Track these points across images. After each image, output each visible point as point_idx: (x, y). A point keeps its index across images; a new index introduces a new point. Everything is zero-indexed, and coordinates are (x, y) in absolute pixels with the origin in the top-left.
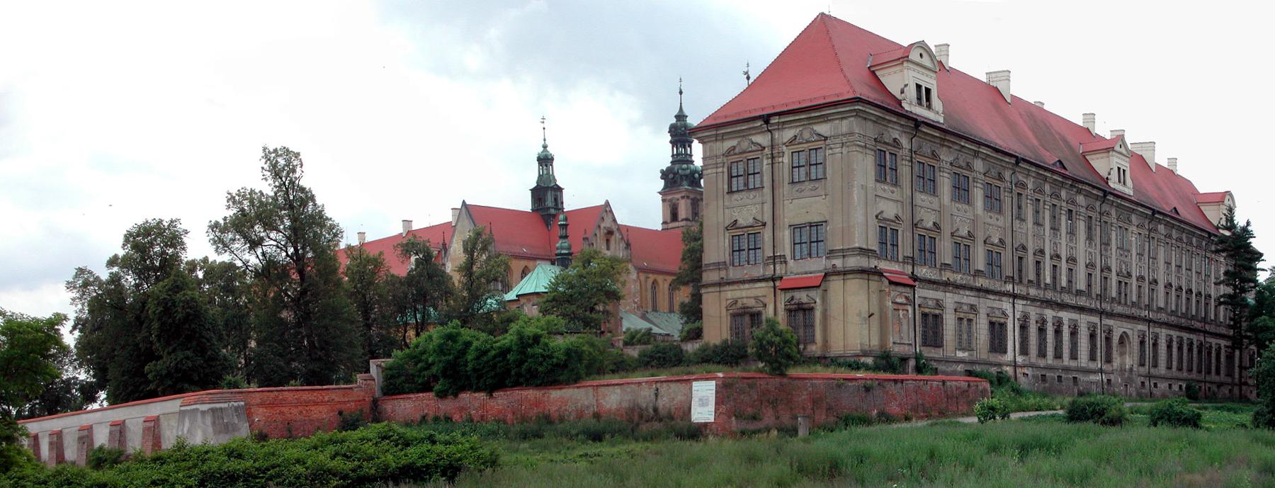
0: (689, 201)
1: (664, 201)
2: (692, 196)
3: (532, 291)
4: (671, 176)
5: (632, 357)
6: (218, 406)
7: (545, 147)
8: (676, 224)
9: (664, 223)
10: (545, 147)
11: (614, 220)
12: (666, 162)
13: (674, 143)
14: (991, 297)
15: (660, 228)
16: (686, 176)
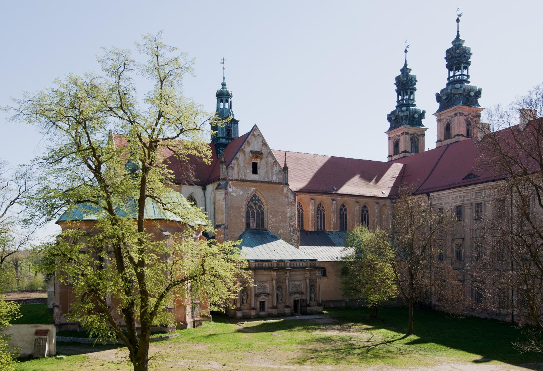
0: (408, 137)
1: (438, 121)
7: (224, 85)
9: (390, 156)
10: (224, 85)
11: (265, 144)
12: (392, 106)
13: (399, 92)
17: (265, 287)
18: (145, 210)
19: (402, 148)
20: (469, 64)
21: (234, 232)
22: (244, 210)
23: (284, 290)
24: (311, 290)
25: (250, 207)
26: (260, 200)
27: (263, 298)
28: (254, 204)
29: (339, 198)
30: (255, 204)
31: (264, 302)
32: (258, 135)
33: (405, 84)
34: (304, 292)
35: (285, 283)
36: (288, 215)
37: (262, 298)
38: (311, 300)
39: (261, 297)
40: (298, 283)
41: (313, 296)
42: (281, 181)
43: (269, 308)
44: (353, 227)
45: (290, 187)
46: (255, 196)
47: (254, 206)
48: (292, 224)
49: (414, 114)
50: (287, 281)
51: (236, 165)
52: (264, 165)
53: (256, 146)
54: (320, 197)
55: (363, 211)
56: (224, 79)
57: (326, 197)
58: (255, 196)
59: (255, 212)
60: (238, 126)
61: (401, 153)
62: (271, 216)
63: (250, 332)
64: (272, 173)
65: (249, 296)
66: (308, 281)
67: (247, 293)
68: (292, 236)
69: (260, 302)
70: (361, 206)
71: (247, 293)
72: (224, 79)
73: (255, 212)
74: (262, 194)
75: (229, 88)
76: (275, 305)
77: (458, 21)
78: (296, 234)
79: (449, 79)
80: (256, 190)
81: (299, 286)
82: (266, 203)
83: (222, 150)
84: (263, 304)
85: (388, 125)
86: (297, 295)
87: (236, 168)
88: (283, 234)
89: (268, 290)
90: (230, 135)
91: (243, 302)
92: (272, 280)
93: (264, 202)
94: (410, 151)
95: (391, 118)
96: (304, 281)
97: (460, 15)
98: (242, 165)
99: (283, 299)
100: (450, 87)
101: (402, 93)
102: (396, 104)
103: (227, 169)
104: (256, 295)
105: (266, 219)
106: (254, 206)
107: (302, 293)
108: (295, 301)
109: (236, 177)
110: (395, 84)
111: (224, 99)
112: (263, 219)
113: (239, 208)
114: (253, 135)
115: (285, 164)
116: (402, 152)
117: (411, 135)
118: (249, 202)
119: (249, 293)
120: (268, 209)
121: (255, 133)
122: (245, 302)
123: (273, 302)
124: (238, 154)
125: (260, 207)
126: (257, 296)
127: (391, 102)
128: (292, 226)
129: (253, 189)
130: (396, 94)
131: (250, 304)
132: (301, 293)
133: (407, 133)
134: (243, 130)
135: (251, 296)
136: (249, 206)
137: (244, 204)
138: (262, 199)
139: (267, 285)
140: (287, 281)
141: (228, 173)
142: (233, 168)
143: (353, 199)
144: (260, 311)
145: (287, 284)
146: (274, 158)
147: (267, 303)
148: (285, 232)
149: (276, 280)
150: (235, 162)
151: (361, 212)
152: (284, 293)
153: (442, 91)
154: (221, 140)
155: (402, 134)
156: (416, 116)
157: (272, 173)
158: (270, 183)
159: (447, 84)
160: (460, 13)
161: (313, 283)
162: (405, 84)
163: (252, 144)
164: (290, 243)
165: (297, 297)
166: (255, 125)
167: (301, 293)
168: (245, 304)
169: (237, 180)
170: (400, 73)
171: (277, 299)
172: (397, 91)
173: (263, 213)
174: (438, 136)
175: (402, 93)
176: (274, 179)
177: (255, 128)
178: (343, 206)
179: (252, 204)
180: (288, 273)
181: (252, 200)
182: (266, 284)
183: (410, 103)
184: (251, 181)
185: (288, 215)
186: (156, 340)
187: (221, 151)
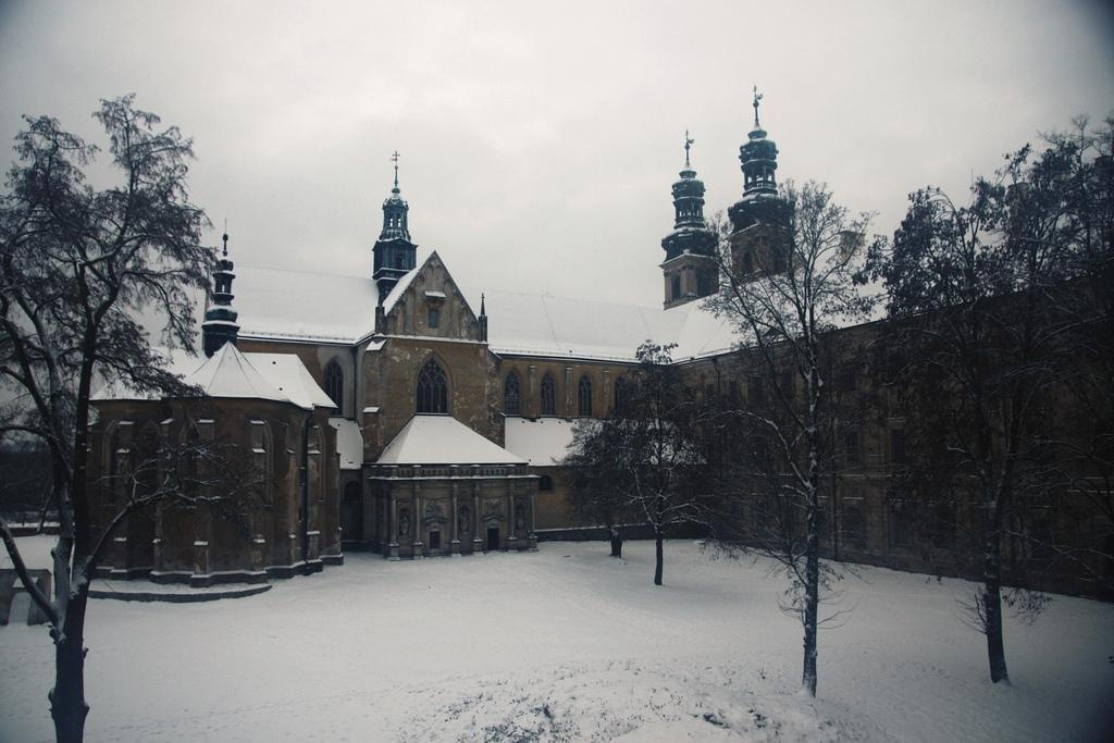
0: (692, 272)
1: (666, 275)
7: (396, 191)
10: (396, 191)
12: (668, 226)
17: (438, 509)
20: (775, 166)
22: (412, 384)
27: (435, 527)
30: (432, 374)
31: (497, 530)
33: (688, 195)
35: (473, 501)
36: (487, 391)
39: (433, 525)
40: (495, 501)
41: (521, 522)
44: (59, 555)
46: (432, 361)
48: (493, 406)
50: (477, 499)
51: (401, 314)
55: (617, 385)
56: (396, 182)
63: (917, 572)
64: (460, 325)
66: (512, 498)
69: (431, 533)
72: (396, 182)
73: (432, 386)
74: (442, 359)
75: (403, 196)
77: (756, 105)
80: (434, 353)
81: (497, 505)
88: (477, 423)
89: (445, 513)
91: (401, 533)
92: (451, 496)
93: (447, 372)
97: (691, 142)
98: (410, 313)
104: (422, 521)
105: (449, 398)
108: (490, 530)
115: (483, 312)
119: (412, 517)
120: (452, 382)
121: (433, 263)
122: (405, 532)
125: (440, 379)
127: (666, 221)
128: (493, 410)
129: (428, 351)
130: (674, 208)
133: (691, 267)
135: (416, 522)
136: (422, 379)
137: (413, 374)
138: (444, 367)
139: (443, 505)
140: (477, 499)
141: (386, 326)
144: (431, 547)
145: (477, 504)
146: (463, 301)
149: (458, 496)
151: (613, 385)
152: (471, 519)
155: (684, 268)
157: (460, 325)
160: (758, 93)
162: (688, 195)
164: (489, 439)
166: (435, 253)
168: (465, 533)
173: (444, 386)
178: (585, 377)
181: (426, 367)
182: (440, 504)
183: (698, 220)
185: (487, 391)
186: (102, 596)
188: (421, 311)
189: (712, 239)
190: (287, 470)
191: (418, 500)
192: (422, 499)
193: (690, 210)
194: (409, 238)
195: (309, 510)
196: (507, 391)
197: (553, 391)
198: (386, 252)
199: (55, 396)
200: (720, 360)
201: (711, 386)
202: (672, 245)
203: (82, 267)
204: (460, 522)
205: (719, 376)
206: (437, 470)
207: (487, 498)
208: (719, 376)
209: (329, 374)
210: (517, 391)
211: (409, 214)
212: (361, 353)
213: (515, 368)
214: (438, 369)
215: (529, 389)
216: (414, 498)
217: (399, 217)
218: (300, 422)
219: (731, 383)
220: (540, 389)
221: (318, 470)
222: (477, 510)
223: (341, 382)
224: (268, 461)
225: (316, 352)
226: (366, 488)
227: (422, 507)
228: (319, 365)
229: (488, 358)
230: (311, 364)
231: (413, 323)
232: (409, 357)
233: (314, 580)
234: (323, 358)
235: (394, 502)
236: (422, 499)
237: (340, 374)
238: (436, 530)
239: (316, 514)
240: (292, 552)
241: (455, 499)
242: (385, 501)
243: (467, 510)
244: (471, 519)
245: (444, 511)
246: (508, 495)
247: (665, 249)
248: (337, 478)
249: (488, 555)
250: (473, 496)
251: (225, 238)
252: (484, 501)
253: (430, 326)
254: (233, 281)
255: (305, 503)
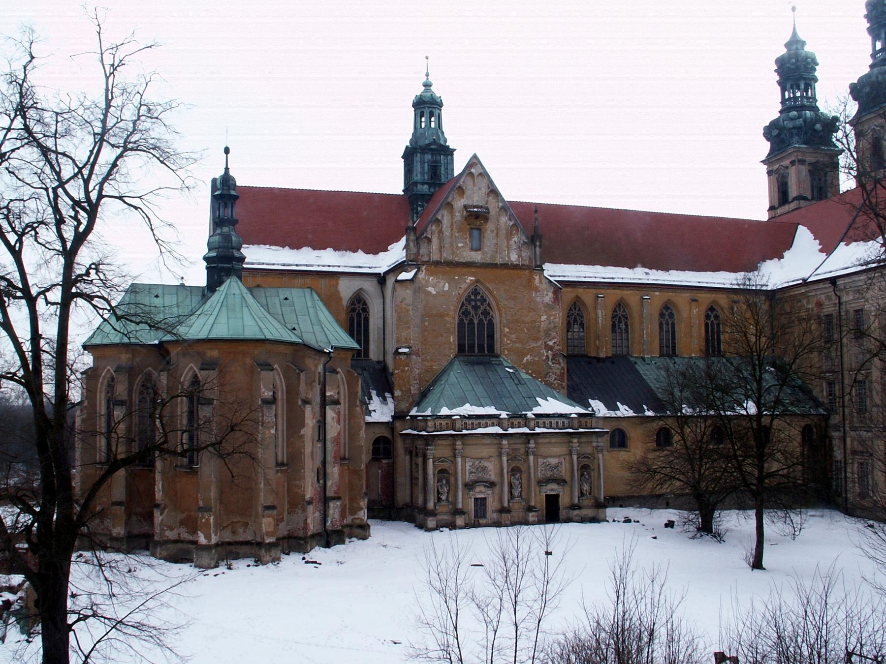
0: (804, 169)
1: (769, 173)
2: (810, 159)
3: (203, 335)
4: (775, 132)
5: (341, 474)
6: (469, 432)
7: (427, 85)
8: (786, 208)
9: (772, 208)
10: (427, 85)
11: (494, 192)
12: (772, 110)
13: (783, 85)
14: (319, 445)
15: (764, 216)
16: (799, 128)
17: (484, 469)
18: (754, 551)
19: (793, 192)
21: (432, 361)
22: (452, 320)
23: (524, 476)
24: (582, 475)
25: (466, 313)
26: (485, 300)
27: (480, 492)
28: (473, 307)
29: (657, 293)
30: (476, 308)
32: (481, 174)
33: (796, 72)
34: (568, 479)
35: (527, 461)
37: (480, 492)
38: (582, 494)
39: (478, 489)
40: (554, 461)
41: (586, 487)
42: (527, 263)
43: (493, 512)
45: (546, 274)
46: (476, 292)
47: (472, 312)
48: (551, 343)
49: (814, 125)
50: (531, 458)
52: (492, 231)
53: (475, 197)
54: (619, 292)
55: (707, 317)
56: (427, 75)
57: (628, 292)
58: (476, 292)
59: (476, 322)
60: (452, 160)
61: (792, 201)
62: (507, 330)
65: (453, 488)
66: (575, 457)
67: (448, 482)
68: (550, 368)
69: (476, 499)
70: (703, 308)
71: (448, 482)
72: (427, 75)
73: (476, 322)
75: (437, 91)
76: (506, 505)
78: (559, 363)
79: (873, 56)
80: (477, 281)
81: (557, 466)
82: (497, 305)
83: (422, 206)
84: (481, 503)
85: (764, 147)
86: (554, 486)
87: (435, 241)
89: (493, 476)
90: (439, 178)
91: (439, 499)
93: (493, 304)
94: (810, 197)
95: (770, 133)
96: (567, 458)
98: (447, 233)
99: (523, 493)
100: (876, 70)
101: (788, 86)
102: (780, 107)
103: (418, 243)
105: (497, 336)
106: (472, 312)
107: (564, 481)
109: (435, 257)
110: (776, 71)
111: (427, 112)
112: (491, 337)
113: (442, 316)
114: (471, 174)
116: (795, 199)
117: (809, 164)
118: (463, 305)
119: (452, 479)
121: (473, 170)
122: (444, 497)
123: (501, 500)
124: (440, 213)
125: (486, 313)
126: (469, 486)
127: (769, 105)
130: (779, 88)
131: (455, 503)
132: (561, 481)
133: (802, 162)
134: (459, 166)
135: (456, 487)
141: (419, 249)
142: (429, 240)
143: (687, 295)
145: (532, 464)
147: (490, 501)
148: (537, 359)
149: (508, 454)
150: (434, 228)
151: (703, 318)
152: (524, 481)
153: (860, 80)
154: (420, 187)
155: (793, 163)
156: (818, 126)
158: (506, 266)
159: (871, 66)
161: (585, 461)
162: (796, 72)
163: (468, 193)
165: (552, 490)
166: (475, 157)
167: (561, 481)
168: (444, 503)
169: (437, 263)
170: (784, 51)
171: (511, 493)
172: (779, 83)
173: (491, 324)
174: (771, 201)
175: (788, 86)
176: (514, 257)
177: (475, 161)
179: (469, 308)
180: (532, 441)
181: (468, 299)
184: (469, 265)
187: (419, 209)
188: (460, 230)
189: (831, 124)
190: (303, 424)
191: (459, 460)
192: (464, 458)
193: (799, 89)
194: (446, 141)
195: (329, 470)
196: (569, 326)
197: (626, 325)
198: (418, 158)
199: (809, 296)
200: (840, 282)
201: (829, 316)
202: (776, 134)
203: (55, 190)
204: (511, 486)
205: (840, 304)
206: (554, 421)
207: (545, 457)
208: (840, 304)
209: (353, 310)
210: (582, 325)
211: (444, 111)
212: (390, 282)
213: (578, 297)
214: (483, 300)
215: (597, 322)
216: (455, 456)
217: (431, 115)
218: (316, 366)
219: (856, 311)
220: (610, 324)
221: (339, 422)
222: (532, 471)
223: (367, 320)
224: (280, 412)
225: (337, 284)
226: (400, 445)
227: (464, 469)
228: (340, 299)
229: (545, 285)
230: (330, 301)
231: (452, 246)
232: (446, 288)
233: (351, 552)
234: (346, 290)
235: (431, 461)
236: (464, 458)
237: (365, 310)
238: (482, 496)
239: (336, 476)
240: (309, 521)
241: (505, 459)
242: (420, 460)
243: (520, 471)
244: (524, 481)
245: (492, 473)
246: (570, 454)
247: (768, 140)
248: (362, 433)
249: (832, 527)
250: (527, 454)
251: (227, 151)
252: (541, 461)
253: (472, 250)
254: (764, 158)
255: (324, 462)
